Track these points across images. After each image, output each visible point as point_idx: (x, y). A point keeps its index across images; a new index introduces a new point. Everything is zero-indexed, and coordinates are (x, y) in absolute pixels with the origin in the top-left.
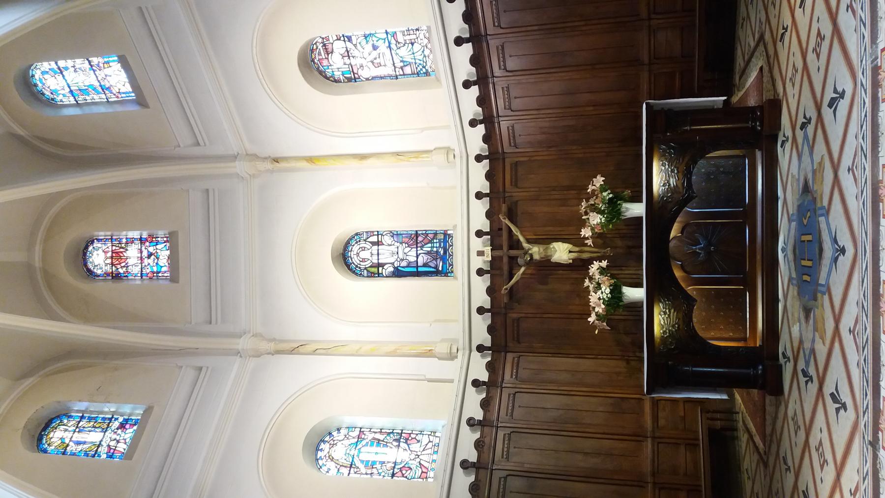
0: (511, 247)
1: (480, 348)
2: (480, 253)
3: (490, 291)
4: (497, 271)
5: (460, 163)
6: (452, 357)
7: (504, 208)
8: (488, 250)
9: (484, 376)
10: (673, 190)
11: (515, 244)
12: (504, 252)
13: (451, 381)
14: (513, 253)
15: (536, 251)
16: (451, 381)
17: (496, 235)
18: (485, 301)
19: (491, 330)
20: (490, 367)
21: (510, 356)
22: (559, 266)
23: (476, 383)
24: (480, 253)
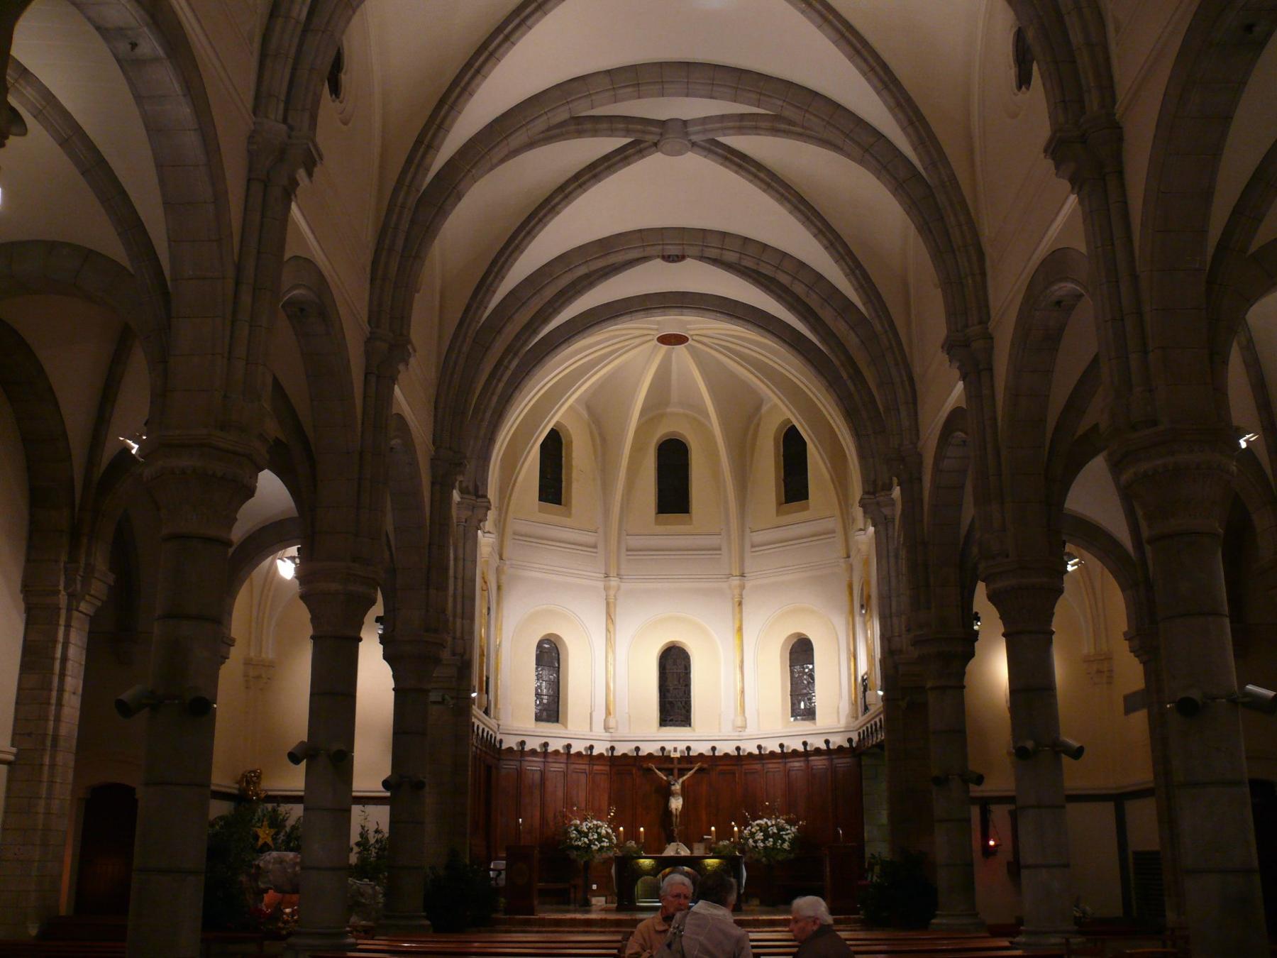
0: (680, 770)
1: (612, 748)
2: (675, 750)
3: (650, 755)
4: (663, 759)
5: (735, 735)
6: (606, 728)
7: (705, 766)
8: (678, 755)
9: (595, 752)
10: (705, 868)
11: (682, 772)
12: (676, 766)
13: (834, 532)
14: (676, 772)
15: (677, 787)
16: (834, 532)
17: (688, 759)
18: (643, 752)
19: (625, 755)
20: (601, 755)
21: (607, 768)
22: (667, 802)
23: (591, 747)
24: (675, 750)
